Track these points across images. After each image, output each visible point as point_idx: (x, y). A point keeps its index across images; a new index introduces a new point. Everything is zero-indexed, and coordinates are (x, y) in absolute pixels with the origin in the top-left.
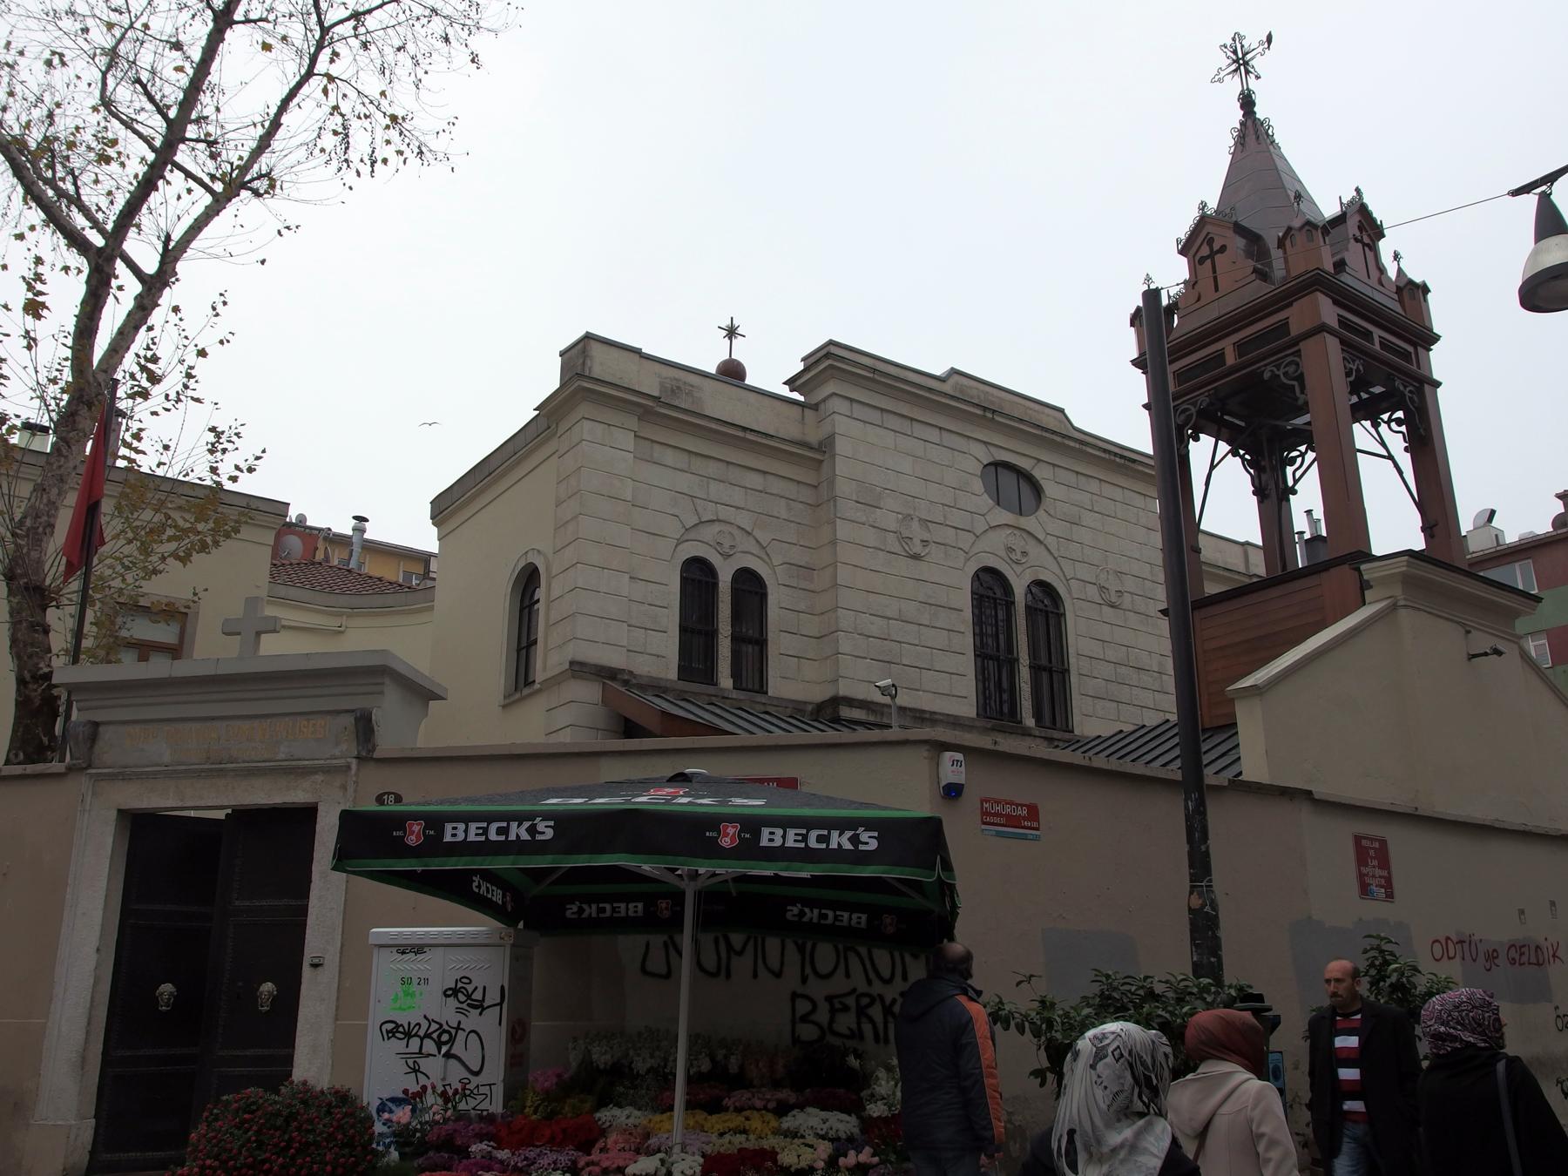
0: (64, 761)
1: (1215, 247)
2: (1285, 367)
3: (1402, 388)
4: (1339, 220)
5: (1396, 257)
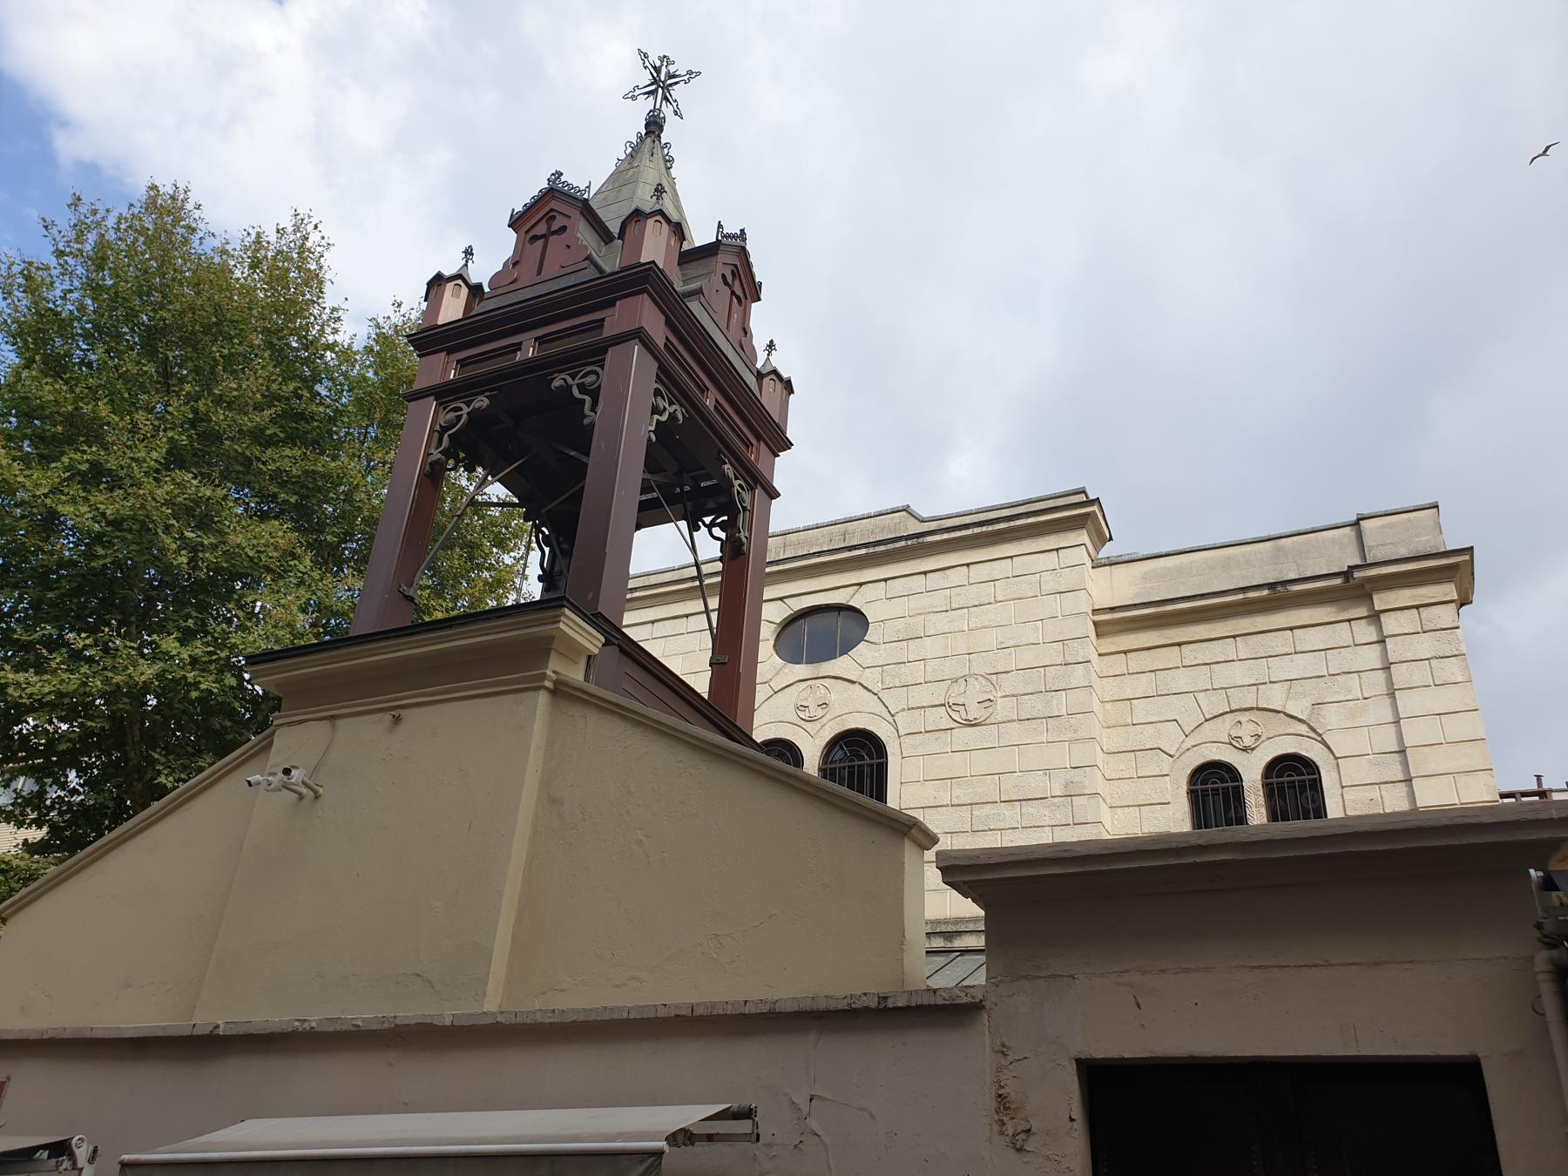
0: (1501, 798)
1: (555, 226)
2: (582, 378)
4: (710, 250)
5: (771, 346)
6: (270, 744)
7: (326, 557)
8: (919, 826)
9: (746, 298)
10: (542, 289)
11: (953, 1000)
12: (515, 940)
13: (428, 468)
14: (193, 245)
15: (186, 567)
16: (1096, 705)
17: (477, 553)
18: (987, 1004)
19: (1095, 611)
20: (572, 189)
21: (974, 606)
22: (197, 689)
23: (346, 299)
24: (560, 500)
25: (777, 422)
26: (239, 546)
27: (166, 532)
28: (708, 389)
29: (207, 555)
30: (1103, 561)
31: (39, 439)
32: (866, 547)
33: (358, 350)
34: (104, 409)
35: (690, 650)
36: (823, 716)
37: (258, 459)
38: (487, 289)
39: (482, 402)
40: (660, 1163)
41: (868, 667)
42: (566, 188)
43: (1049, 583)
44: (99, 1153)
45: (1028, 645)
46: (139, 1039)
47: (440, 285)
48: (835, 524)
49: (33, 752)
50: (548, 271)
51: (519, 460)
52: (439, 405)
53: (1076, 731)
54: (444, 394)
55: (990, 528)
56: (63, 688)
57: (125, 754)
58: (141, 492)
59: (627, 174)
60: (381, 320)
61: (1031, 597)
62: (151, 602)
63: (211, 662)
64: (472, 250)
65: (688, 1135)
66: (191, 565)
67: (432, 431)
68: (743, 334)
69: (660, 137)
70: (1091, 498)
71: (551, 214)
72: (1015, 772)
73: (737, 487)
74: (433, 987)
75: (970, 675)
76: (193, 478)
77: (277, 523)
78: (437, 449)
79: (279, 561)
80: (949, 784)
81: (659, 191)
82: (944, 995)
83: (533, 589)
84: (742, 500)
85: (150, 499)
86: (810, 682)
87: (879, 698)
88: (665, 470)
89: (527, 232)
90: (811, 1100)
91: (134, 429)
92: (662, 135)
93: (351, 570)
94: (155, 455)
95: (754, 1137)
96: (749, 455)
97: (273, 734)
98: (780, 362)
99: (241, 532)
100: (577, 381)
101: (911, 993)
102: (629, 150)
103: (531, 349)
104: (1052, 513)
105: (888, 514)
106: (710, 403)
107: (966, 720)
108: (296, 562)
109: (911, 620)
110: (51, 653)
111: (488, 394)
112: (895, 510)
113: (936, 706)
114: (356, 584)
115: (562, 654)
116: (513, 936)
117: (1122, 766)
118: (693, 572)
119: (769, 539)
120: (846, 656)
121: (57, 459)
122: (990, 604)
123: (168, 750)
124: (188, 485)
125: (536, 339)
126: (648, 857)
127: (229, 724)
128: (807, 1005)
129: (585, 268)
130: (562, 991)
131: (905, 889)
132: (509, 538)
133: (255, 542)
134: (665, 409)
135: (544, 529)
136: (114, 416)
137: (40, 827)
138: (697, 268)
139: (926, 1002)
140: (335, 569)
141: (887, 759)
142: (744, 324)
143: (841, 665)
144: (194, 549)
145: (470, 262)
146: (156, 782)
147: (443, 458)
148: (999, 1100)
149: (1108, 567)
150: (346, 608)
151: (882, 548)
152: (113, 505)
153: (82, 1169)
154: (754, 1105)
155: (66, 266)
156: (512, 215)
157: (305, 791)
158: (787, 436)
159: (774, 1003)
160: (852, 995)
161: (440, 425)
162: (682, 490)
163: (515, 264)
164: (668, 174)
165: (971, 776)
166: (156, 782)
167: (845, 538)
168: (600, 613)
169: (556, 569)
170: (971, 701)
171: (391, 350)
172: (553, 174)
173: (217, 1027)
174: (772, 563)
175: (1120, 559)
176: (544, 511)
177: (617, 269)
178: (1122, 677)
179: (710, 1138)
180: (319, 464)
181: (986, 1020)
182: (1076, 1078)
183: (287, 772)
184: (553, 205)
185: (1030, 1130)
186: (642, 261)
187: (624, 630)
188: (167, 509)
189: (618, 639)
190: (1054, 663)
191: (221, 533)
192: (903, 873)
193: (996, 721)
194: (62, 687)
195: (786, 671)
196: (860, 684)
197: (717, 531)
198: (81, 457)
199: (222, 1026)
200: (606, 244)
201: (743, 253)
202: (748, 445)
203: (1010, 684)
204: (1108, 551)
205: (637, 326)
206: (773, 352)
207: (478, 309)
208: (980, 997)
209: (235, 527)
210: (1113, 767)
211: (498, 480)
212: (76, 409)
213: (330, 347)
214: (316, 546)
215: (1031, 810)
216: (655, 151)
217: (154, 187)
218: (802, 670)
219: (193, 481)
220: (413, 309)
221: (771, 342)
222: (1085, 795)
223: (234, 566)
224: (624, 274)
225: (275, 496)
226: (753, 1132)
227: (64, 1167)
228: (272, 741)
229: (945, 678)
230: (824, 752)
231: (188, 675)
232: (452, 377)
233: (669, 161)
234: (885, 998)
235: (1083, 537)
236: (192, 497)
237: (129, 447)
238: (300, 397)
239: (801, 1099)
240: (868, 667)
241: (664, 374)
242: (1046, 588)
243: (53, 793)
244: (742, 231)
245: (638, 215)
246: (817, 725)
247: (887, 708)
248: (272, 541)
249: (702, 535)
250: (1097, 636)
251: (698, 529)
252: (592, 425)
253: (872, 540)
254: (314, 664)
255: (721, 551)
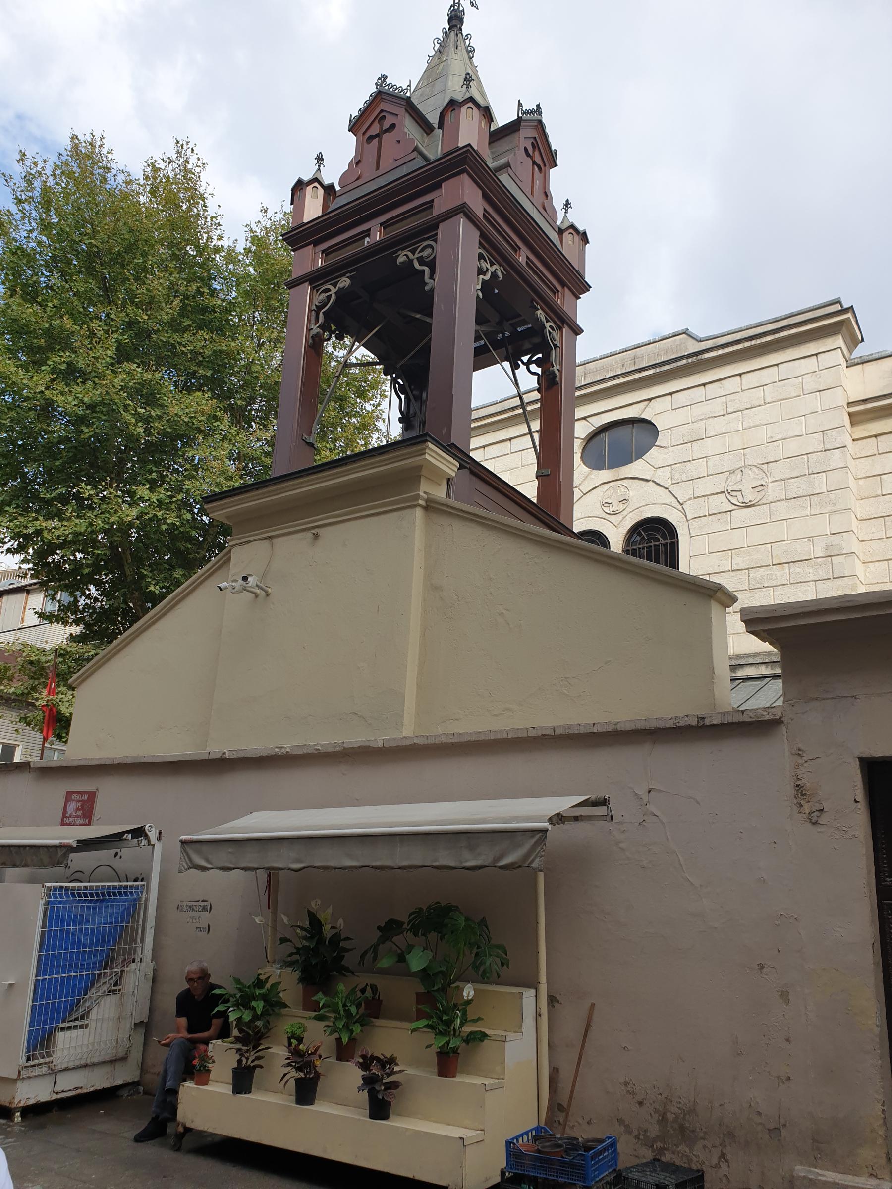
1: (386, 125)
2: (419, 252)
3: (543, 319)
4: (513, 127)
5: (567, 204)
6: (229, 559)
7: (238, 417)
8: (723, 590)
9: (545, 166)
10: (382, 182)
11: (758, 718)
12: (419, 686)
13: (311, 341)
14: (109, 182)
15: (143, 434)
16: (851, 482)
17: (346, 405)
18: (785, 720)
19: (850, 404)
20: (396, 89)
21: (747, 409)
22: (165, 523)
23: (219, 206)
24: (411, 355)
25: (577, 269)
26: (176, 414)
27: (125, 410)
28: (520, 249)
29: (156, 424)
30: (856, 361)
31: (31, 350)
32: (653, 368)
33: (240, 252)
34: (68, 323)
35: (514, 467)
36: (624, 510)
37: (180, 344)
38: (338, 188)
39: (345, 282)
40: (546, 838)
41: (659, 468)
42: (391, 90)
43: (810, 383)
44: (163, 834)
45: (793, 437)
46: (175, 763)
47: (302, 189)
48: (626, 351)
49: (64, 574)
50: (385, 166)
51: (376, 327)
52: (313, 288)
53: (835, 504)
54: (315, 279)
55: (758, 341)
56: (78, 529)
57: (124, 573)
58: (104, 382)
59: (438, 69)
60: (253, 226)
61: (795, 397)
62: (122, 462)
63: (171, 503)
64: (322, 156)
65: (560, 817)
66: (147, 433)
67: (310, 310)
68: (545, 198)
69: (461, 30)
70: (845, 306)
71: (382, 114)
72: (785, 541)
73: (548, 329)
74: (366, 721)
75: (745, 466)
76: (137, 367)
77: (200, 394)
78: (315, 325)
79: (206, 423)
80: (730, 554)
81: (468, 80)
82: (750, 714)
83: (396, 430)
84: (553, 339)
85: (111, 387)
86: (612, 484)
87: (669, 491)
88: (489, 321)
89: (364, 134)
90: (649, 791)
91: (92, 334)
92: (462, 28)
93: (258, 425)
94: (109, 353)
95: (609, 818)
96: (556, 300)
97: (230, 552)
98: (576, 218)
99: (177, 404)
100: (417, 255)
101: (724, 714)
102: (437, 46)
103: (378, 233)
104: (811, 323)
105: (670, 337)
106: (522, 259)
107: (743, 503)
108: (218, 423)
109: (695, 426)
110: (64, 505)
111: (348, 275)
112: (676, 333)
113: (717, 494)
114: (263, 435)
115: (429, 479)
116: (417, 684)
117: (873, 530)
118: (517, 401)
119: (577, 368)
120: (641, 460)
121: (46, 364)
122: (760, 406)
123: (152, 568)
124: (135, 372)
125: (381, 224)
126: (508, 624)
127: (190, 546)
128: (641, 725)
129: (415, 158)
130: (457, 720)
131: (713, 638)
132: (368, 390)
133: (187, 410)
134: (487, 269)
135: (400, 381)
136: (76, 327)
137: (78, 625)
138: (504, 145)
139: (735, 720)
140: (246, 426)
141: (678, 538)
142: (545, 189)
143: (637, 468)
144: (147, 420)
145: (322, 166)
146: (148, 590)
147: (321, 331)
148: (797, 789)
149: (861, 365)
150: (259, 454)
151: (667, 367)
152: (89, 393)
153: (154, 845)
154: (607, 796)
155: (25, 211)
156: (350, 120)
157: (258, 591)
158: (586, 280)
159: (616, 724)
160: (676, 717)
161: (316, 305)
162: (503, 335)
163: (358, 163)
164: (471, 63)
165: (748, 547)
166: (148, 590)
167: (635, 362)
168: (453, 444)
169: (411, 412)
170: (746, 487)
171: (263, 249)
172: (379, 79)
173: (224, 753)
174: (580, 388)
175: (871, 358)
176: (398, 366)
177: (439, 155)
178: (873, 457)
179: (576, 819)
180: (223, 345)
181: (785, 733)
182: (859, 771)
183: (245, 578)
184: (383, 106)
185: (823, 809)
186: (460, 145)
187: (472, 454)
188: (124, 393)
189: (468, 463)
190: (816, 450)
191: (162, 406)
192: (711, 627)
193: (768, 502)
194: (76, 529)
195: (592, 476)
196: (653, 481)
197: (534, 368)
198: (59, 359)
199: (227, 752)
200: (428, 134)
201: (540, 126)
202: (555, 291)
203: (779, 471)
204: (861, 351)
205: (460, 203)
206: (569, 209)
207: (333, 206)
208: (780, 715)
209: (172, 401)
210: (863, 531)
211: (362, 345)
212: (51, 325)
213: (217, 250)
214: (230, 408)
215: (798, 570)
216: (459, 43)
217: (74, 137)
218: (605, 475)
219: (138, 369)
220: (276, 213)
221: (567, 201)
222: (842, 555)
223: (175, 430)
224: (446, 159)
225: (195, 372)
226: (608, 815)
227: (143, 844)
228: (230, 557)
229: (724, 470)
230: (627, 538)
231: (157, 513)
232: (319, 265)
233: (471, 51)
234: (704, 718)
235: (838, 341)
236: (139, 381)
237: (91, 349)
238: (202, 294)
239: (642, 791)
240: (659, 468)
241: (485, 240)
242: (808, 388)
243: (82, 602)
244: (538, 106)
245: (453, 105)
246: (620, 517)
247: (676, 498)
248: (199, 408)
249: (522, 371)
250: (851, 425)
251: (518, 367)
252: (432, 290)
253: (657, 362)
254: (253, 499)
255: (538, 383)
